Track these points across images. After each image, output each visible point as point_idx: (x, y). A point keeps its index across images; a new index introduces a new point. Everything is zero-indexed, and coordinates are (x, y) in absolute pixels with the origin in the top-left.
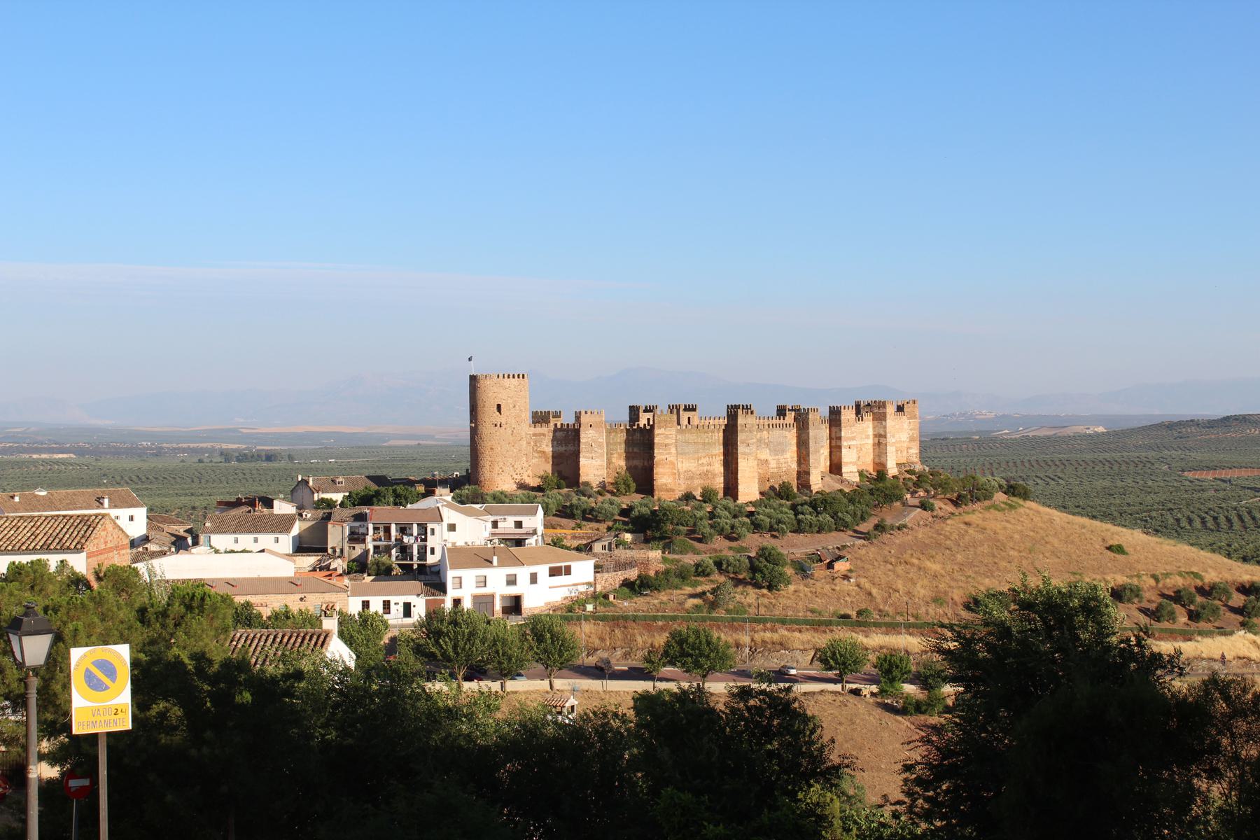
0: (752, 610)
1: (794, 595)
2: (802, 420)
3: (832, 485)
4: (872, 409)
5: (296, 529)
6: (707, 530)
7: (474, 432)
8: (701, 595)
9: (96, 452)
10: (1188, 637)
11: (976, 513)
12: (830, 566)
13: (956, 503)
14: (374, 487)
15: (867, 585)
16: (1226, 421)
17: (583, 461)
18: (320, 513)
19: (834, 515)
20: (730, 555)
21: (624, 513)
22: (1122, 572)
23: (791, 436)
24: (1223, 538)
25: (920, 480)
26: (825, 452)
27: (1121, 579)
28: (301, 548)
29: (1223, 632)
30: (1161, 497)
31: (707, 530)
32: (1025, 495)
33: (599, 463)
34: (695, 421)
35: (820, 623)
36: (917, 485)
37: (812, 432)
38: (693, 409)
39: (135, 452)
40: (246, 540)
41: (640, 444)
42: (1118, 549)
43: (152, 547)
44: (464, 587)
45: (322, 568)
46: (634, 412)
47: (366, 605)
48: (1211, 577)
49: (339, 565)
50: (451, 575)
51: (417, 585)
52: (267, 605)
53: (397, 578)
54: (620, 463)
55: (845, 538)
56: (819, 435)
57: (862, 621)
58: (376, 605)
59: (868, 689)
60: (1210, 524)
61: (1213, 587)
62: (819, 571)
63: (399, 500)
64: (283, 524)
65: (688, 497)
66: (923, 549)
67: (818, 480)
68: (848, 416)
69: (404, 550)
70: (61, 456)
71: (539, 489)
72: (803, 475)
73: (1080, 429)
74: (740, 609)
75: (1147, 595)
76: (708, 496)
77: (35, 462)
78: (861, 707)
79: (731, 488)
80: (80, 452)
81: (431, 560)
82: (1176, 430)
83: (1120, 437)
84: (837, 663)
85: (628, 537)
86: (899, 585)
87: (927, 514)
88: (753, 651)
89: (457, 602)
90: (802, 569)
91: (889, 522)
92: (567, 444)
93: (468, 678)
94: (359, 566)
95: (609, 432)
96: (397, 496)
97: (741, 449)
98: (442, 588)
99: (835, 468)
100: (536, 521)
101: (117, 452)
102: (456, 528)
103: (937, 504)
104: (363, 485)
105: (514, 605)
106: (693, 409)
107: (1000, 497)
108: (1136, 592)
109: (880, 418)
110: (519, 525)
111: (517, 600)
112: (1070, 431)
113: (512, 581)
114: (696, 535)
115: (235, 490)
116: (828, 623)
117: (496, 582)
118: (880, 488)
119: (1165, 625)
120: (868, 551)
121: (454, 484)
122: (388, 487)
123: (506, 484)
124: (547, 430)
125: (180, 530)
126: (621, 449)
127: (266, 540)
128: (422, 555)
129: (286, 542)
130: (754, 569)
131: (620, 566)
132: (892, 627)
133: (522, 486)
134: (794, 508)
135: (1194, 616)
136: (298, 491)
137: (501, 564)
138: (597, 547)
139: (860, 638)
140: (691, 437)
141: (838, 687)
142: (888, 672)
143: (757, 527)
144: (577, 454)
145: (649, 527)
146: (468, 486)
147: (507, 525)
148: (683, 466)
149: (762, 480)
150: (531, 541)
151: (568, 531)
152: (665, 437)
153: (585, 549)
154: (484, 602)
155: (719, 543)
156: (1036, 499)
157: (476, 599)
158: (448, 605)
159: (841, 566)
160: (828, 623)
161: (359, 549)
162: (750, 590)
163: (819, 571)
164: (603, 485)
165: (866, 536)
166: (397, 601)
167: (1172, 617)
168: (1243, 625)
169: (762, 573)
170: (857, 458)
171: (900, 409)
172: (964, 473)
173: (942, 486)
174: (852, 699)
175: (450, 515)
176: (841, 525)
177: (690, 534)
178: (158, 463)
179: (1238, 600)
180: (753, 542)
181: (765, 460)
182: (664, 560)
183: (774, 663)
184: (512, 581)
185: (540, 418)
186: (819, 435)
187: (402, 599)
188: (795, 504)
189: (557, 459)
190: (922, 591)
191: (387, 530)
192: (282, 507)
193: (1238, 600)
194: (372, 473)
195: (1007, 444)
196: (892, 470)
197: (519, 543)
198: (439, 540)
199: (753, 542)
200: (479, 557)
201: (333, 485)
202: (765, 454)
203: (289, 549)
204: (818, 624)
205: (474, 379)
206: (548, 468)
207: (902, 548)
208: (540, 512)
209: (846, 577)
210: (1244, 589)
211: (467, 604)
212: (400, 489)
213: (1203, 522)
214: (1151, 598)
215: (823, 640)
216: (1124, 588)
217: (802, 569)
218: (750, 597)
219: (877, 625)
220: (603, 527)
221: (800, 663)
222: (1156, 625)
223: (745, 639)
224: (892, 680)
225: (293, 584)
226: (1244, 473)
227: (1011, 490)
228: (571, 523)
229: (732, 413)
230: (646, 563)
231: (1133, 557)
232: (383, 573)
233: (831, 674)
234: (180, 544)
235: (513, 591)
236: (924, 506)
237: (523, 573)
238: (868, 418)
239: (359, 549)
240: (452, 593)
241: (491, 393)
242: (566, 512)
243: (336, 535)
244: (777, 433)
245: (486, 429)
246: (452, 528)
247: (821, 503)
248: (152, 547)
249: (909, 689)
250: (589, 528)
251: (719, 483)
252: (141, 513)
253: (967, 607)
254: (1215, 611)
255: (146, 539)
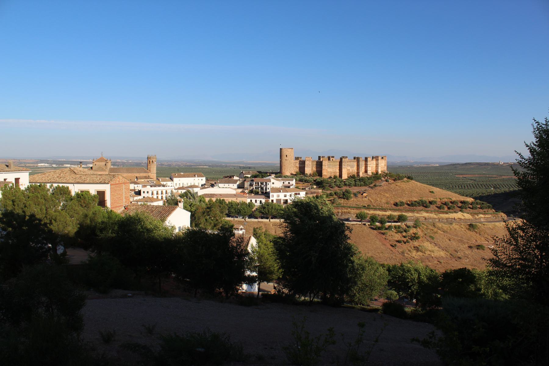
0: (342, 204)
1: (353, 201)
2: (357, 159)
3: (365, 175)
4: (376, 158)
5: (238, 183)
6: (333, 185)
7: (281, 161)
8: (331, 200)
9: (213, 166)
10: (447, 213)
11: (399, 183)
12: (362, 194)
13: (394, 180)
14: (258, 173)
15: (370, 199)
16: (466, 164)
17: (306, 169)
18: (244, 179)
19: (364, 183)
20: (339, 191)
21: (315, 181)
22: (433, 197)
23: (355, 164)
24: (462, 191)
25: (386, 175)
26: (364, 168)
27: (432, 199)
28: (239, 187)
29: (456, 212)
30: (449, 181)
31: (333, 185)
32: (412, 179)
33: (309, 169)
34: (334, 160)
35: (358, 208)
36: (385, 176)
37: (360, 163)
38: (333, 157)
39: (221, 166)
40: (227, 185)
41: (319, 165)
42: (432, 192)
43: (206, 186)
44: (274, 197)
45: (243, 192)
46: (319, 157)
47: (251, 201)
48: (454, 199)
49: (247, 191)
50: (271, 194)
51: (263, 196)
52: (228, 200)
53: (260, 195)
54: (315, 169)
55: (366, 188)
56: (362, 164)
57: (368, 208)
58: (253, 201)
59: (367, 224)
60: (460, 187)
61: (454, 202)
62: (359, 196)
63: (263, 177)
64: (235, 182)
65: (330, 177)
66: (385, 191)
67: (361, 175)
68: (369, 159)
69: (262, 188)
70: (42, 164)
71: (295, 175)
72: (358, 173)
73: (433, 165)
74: (340, 204)
75: (438, 203)
76: (335, 177)
77: (199, 168)
78: (365, 228)
79: (341, 176)
80: (209, 166)
81: (268, 191)
82: (455, 166)
83: (442, 167)
84: (360, 217)
85: (315, 187)
86: (378, 199)
87: (387, 183)
88: (342, 214)
89: (272, 201)
90: (355, 195)
91: (377, 184)
92: (302, 164)
93: (272, 218)
94: (251, 192)
95: (312, 162)
96: (262, 176)
97: (343, 166)
98: (269, 197)
99: (366, 171)
100: (293, 182)
101: (217, 166)
102: (274, 183)
103: (390, 180)
104: (255, 173)
105: (286, 202)
106: (333, 157)
107: (405, 179)
108: (435, 202)
109: (377, 160)
110: (289, 183)
111: (287, 200)
112: (430, 165)
113: (285, 196)
114: (331, 186)
115: (216, 174)
116: (360, 208)
117: (282, 196)
118: (376, 176)
119: (442, 210)
120: (372, 191)
121: (276, 173)
122: (262, 174)
123: (288, 174)
124: (298, 161)
125: (213, 183)
126: (315, 166)
127: (231, 185)
128: (266, 190)
129: (235, 186)
130: (344, 195)
131: (312, 193)
132: (375, 209)
133: (292, 174)
134: (355, 181)
135: (449, 208)
136: (241, 175)
137: (283, 192)
138: (307, 189)
139: (368, 212)
140: (331, 164)
141: (360, 223)
142: (372, 220)
143: (345, 185)
144: (304, 167)
145: (320, 184)
146: (279, 174)
147: (286, 183)
148: (329, 170)
149: (348, 174)
150: (291, 187)
151: (301, 185)
152: (325, 163)
153: (303, 189)
154: (279, 201)
155: (336, 188)
156: (414, 180)
157: (277, 200)
158: (270, 201)
159: (365, 194)
160: (360, 208)
161: (252, 188)
162: (342, 200)
163: (359, 196)
164: (310, 174)
165: (372, 188)
166: (258, 200)
167: (443, 208)
168: (460, 211)
169: (345, 196)
170: (371, 169)
171: (382, 158)
172: (396, 174)
173: (391, 176)
174: (363, 226)
175: (272, 181)
176: (365, 185)
177: (330, 186)
178: (225, 169)
179: (460, 205)
180: (344, 188)
181: (349, 169)
182: (322, 192)
183: (346, 217)
184: (285, 196)
185: (297, 158)
186: (362, 164)
187: (260, 200)
188: (355, 179)
189: (300, 168)
190: (384, 201)
191: (258, 184)
192: (236, 178)
193: (460, 205)
194: (259, 170)
195: (416, 168)
196: (380, 172)
197: (289, 187)
198: (270, 186)
199: (344, 188)
200: (278, 190)
201: (249, 173)
202: (349, 168)
203: (236, 187)
204: (358, 208)
205: (281, 149)
206: (298, 170)
207: (380, 190)
208: (294, 180)
209: (366, 197)
210: (461, 202)
211: (275, 201)
212: (263, 174)
213: (459, 187)
214: (439, 204)
215: (358, 211)
216: (432, 201)
217: (355, 195)
218: (342, 201)
219: (372, 208)
220: (309, 184)
221: (353, 217)
222: (440, 210)
223: (340, 211)
224: (374, 222)
225: (235, 196)
226: (469, 176)
227: (409, 178)
228: (302, 183)
229: (341, 159)
230: (318, 193)
231: (436, 194)
232: (257, 193)
233: (359, 220)
234: (212, 186)
235: (286, 198)
236: (386, 181)
237: (288, 194)
238: (374, 160)
239: (252, 188)
240: (271, 198)
241: (285, 153)
242: (301, 180)
243: (247, 184)
244: (352, 163)
245: (284, 161)
246: (273, 183)
247: (362, 180)
248: (206, 186)
249: (377, 224)
250: (306, 184)
251: (338, 174)
252: (204, 179)
253: (394, 205)
254: (454, 207)
255: (205, 184)
